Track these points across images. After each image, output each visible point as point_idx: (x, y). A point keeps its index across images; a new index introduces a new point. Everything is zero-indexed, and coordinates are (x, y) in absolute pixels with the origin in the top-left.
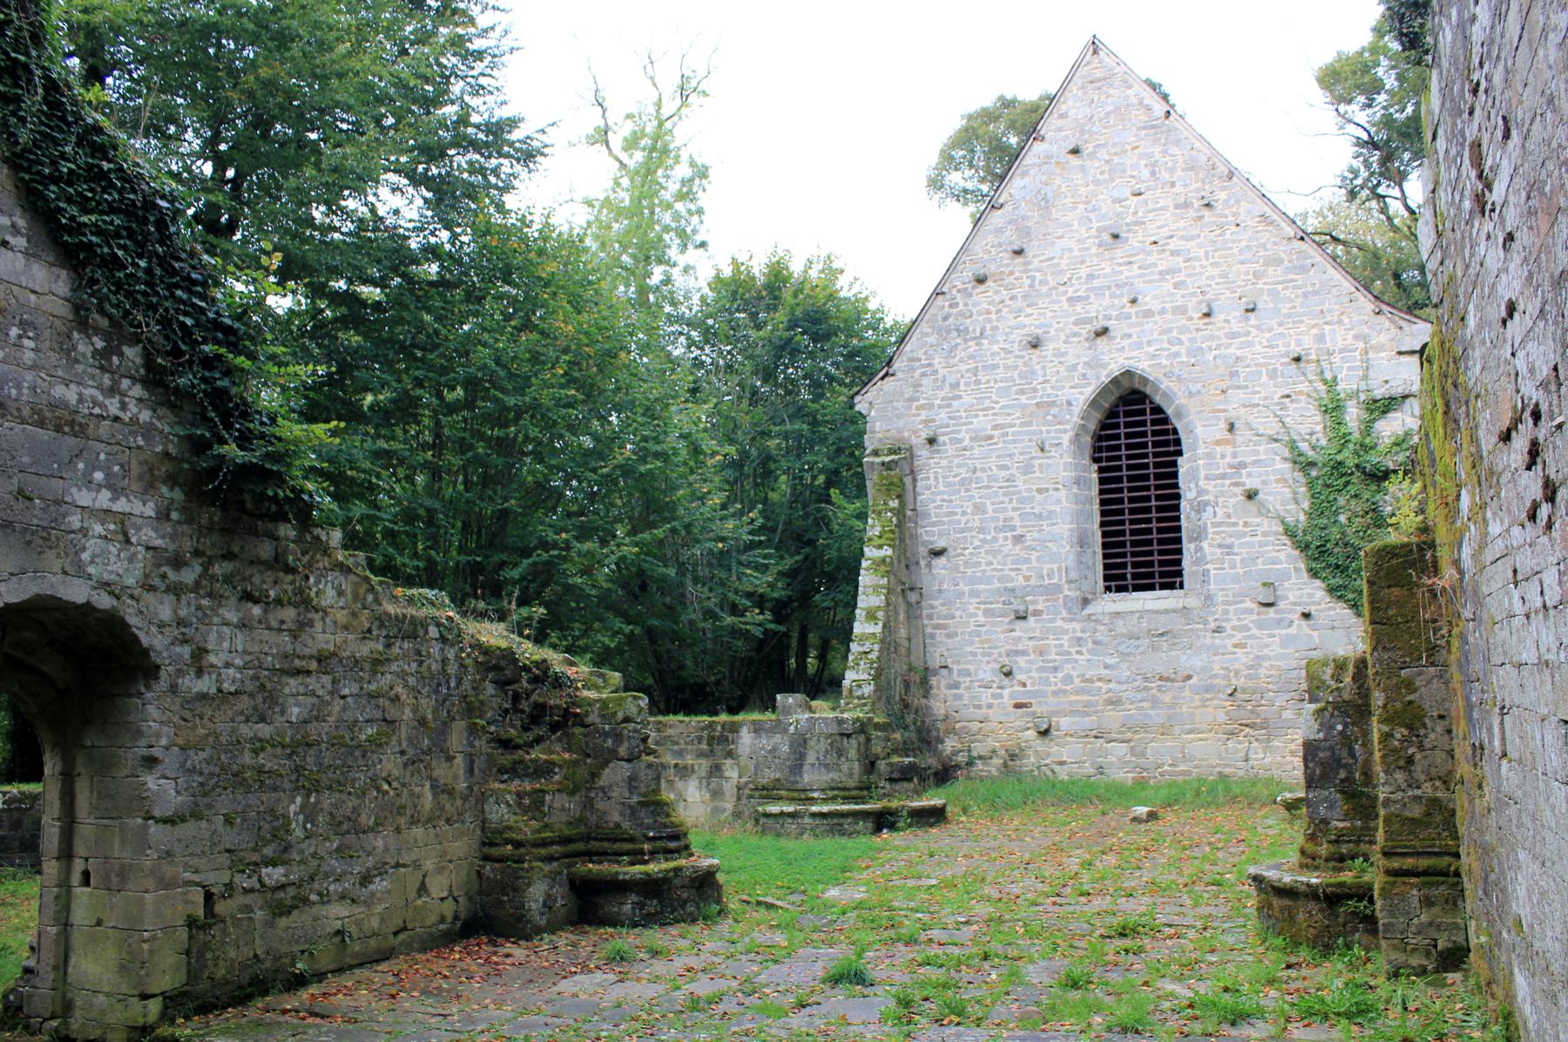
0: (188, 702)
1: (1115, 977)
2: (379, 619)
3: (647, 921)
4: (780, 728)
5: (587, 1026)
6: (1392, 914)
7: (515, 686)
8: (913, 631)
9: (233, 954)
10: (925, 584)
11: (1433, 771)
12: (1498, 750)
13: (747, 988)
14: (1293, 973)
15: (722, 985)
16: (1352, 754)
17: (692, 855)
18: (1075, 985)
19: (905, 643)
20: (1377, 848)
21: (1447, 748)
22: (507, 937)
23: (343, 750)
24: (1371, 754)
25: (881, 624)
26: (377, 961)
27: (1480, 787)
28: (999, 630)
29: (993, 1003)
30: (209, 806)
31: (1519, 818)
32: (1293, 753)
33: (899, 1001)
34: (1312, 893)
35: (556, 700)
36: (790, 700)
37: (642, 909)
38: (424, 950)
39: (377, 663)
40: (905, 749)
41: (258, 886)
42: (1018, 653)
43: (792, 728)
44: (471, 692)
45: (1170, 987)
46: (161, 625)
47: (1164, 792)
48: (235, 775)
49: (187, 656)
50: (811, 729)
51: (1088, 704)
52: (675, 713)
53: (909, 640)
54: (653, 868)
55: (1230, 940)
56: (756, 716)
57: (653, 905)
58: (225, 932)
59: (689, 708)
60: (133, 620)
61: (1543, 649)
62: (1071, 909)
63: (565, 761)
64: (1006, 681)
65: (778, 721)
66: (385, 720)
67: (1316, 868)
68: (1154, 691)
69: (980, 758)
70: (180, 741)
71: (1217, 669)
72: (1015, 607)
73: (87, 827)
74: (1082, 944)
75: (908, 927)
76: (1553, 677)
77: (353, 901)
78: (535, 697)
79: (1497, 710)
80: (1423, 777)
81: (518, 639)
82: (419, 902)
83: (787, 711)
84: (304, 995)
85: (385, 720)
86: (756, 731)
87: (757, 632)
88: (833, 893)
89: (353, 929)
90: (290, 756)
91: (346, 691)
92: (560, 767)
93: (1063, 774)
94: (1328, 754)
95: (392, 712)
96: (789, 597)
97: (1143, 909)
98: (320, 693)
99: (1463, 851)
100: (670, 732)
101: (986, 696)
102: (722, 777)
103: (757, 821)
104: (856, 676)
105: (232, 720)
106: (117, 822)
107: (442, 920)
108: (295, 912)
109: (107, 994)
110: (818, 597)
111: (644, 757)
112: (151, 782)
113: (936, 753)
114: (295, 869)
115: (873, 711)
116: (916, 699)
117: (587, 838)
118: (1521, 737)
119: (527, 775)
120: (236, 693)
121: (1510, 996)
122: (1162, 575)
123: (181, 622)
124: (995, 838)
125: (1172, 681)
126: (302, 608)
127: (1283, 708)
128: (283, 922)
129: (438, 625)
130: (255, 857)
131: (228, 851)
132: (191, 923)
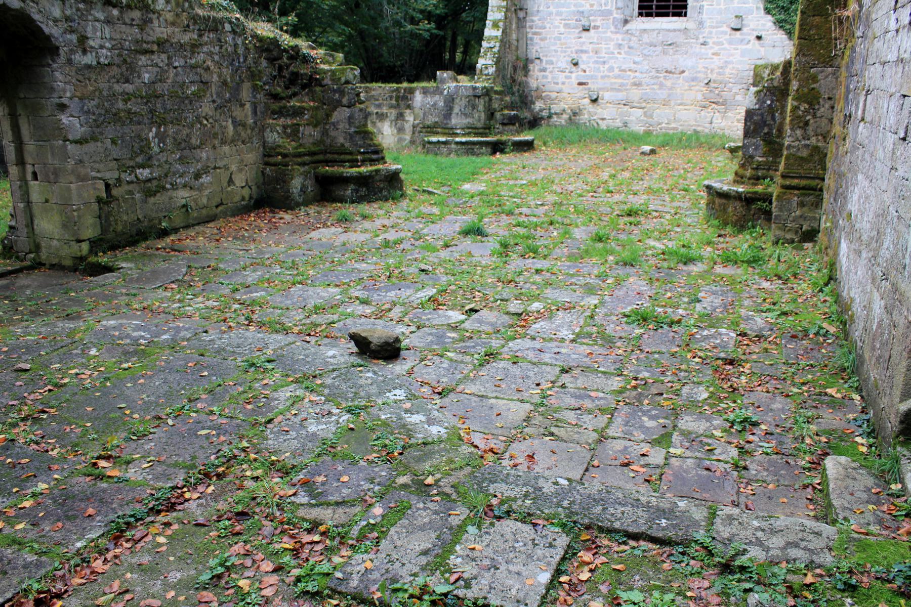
0: (80, 70)
1: (623, 237)
2: (193, 18)
3: (360, 200)
4: (438, 91)
5: (326, 255)
6: (781, 210)
7: (280, 62)
8: (521, 35)
9: (125, 218)
10: (529, 6)
11: (819, 131)
12: (859, 117)
13: (417, 236)
14: (721, 239)
15: (402, 234)
16: (773, 119)
17: (386, 163)
18: (600, 240)
19: (515, 43)
20: (779, 173)
21: (830, 117)
22: (280, 209)
23: (178, 100)
24: (785, 119)
25: (501, 30)
26: (208, 222)
27: (844, 139)
28: (572, 37)
29: (554, 248)
30: (101, 134)
31: (863, 156)
32: (738, 121)
33: (501, 245)
34: (738, 197)
35: (304, 70)
36: (445, 75)
37: (357, 193)
38: (233, 216)
39: (195, 47)
40: (511, 107)
41: (135, 180)
42: (582, 51)
43: (446, 92)
44: (252, 65)
45: (652, 243)
46: (56, 21)
47: (661, 139)
48: (115, 115)
49: (75, 41)
50: (457, 92)
51: (622, 85)
52: (377, 82)
53: (518, 41)
54: (363, 169)
55: (689, 220)
56: (424, 84)
57: (363, 191)
58: (119, 206)
59: (385, 80)
60: (36, 17)
61: (902, 51)
62: (602, 199)
63: (311, 107)
64: (574, 69)
65: (437, 87)
66: (202, 82)
67: (743, 183)
68: (661, 79)
69: (556, 114)
70: (78, 94)
71: (700, 68)
72: (583, 23)
73: (30, 147)
74: (606, 219)
75: (508, 206)
76: (904, 68)
77: (191, 188)
78: (291, 68)
79: (864, 93)
80: (812, 134)
81: (280, 33)
82: (229, 189)
83: (443, 81)
84: (168, 240)
85: (202, 82)
86: (424, 93)
87: (426, 35)
88: (467, 186)
89: (192, 204)
90: (146, 104)
91: (177, 64)
92: (308, 110)
93: (603, 125)
94: (759, 117)
95: (206, 77)
96: (446, 14)
97: (642, 201)
98: (161, 65)
99: (826, 177)
100: (373, 93)
101: (561, 77)
102: (404, 120)
103: (424, 146)
104: (485, 62)
105: (109, 82)
106: (47, 143)
107: (243, 199)
108: (159, 195)
109: (58, 240)
110: (464, 15)
111: (357, 105)
112: (65, 119)
113: (530, 110)
114: (156, 170)
115: (494, 83)
116: (520, 77)
117: (325, 152)
118: (875, 108)
119: (288, 115)
120: (109, 65)
121: (836, 254)
122: (675, 7)
123: (68, 19)
124: (561, 160)
125: (673, 73)
126: (144, 11)
127: (736, 94)
128: (152, 200)
129: (231, 23)
130: (132, 163)
131: (115, 160)
132: (99, 200)
